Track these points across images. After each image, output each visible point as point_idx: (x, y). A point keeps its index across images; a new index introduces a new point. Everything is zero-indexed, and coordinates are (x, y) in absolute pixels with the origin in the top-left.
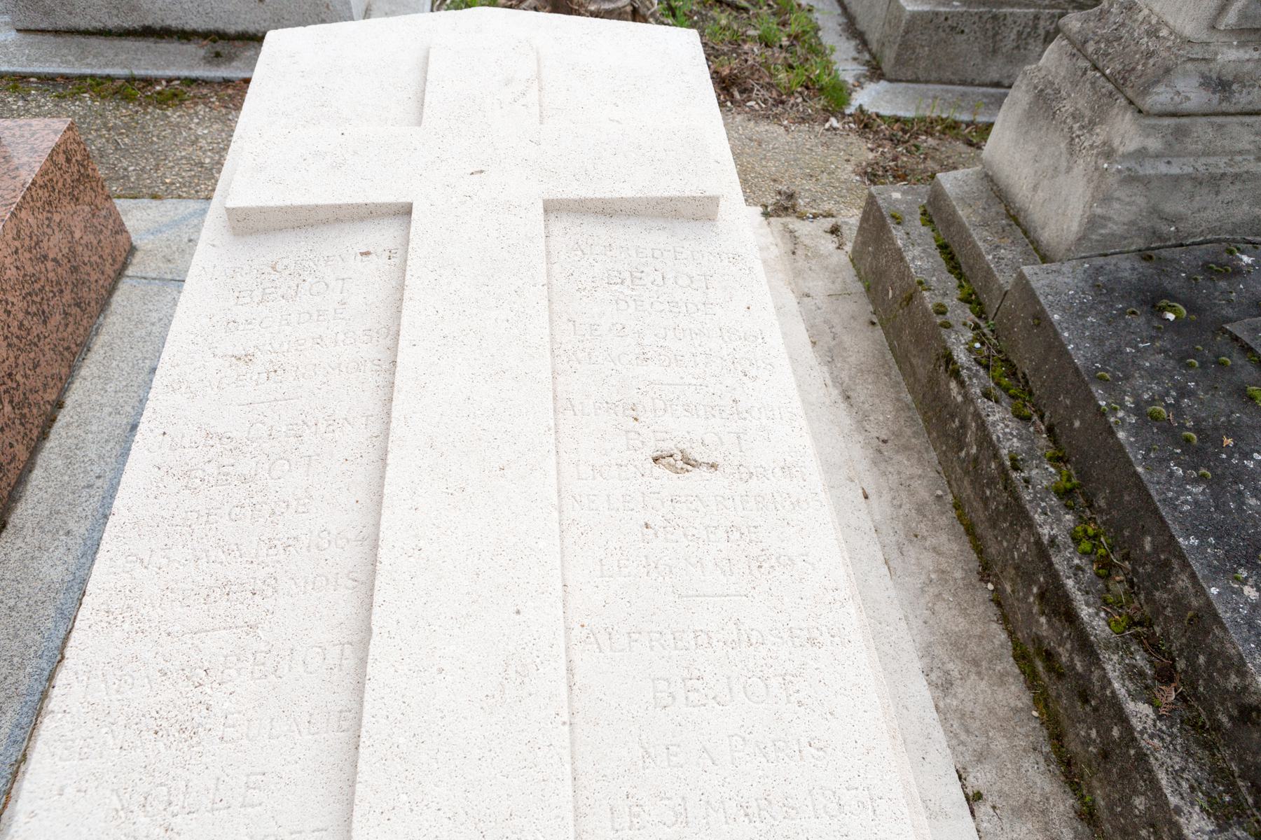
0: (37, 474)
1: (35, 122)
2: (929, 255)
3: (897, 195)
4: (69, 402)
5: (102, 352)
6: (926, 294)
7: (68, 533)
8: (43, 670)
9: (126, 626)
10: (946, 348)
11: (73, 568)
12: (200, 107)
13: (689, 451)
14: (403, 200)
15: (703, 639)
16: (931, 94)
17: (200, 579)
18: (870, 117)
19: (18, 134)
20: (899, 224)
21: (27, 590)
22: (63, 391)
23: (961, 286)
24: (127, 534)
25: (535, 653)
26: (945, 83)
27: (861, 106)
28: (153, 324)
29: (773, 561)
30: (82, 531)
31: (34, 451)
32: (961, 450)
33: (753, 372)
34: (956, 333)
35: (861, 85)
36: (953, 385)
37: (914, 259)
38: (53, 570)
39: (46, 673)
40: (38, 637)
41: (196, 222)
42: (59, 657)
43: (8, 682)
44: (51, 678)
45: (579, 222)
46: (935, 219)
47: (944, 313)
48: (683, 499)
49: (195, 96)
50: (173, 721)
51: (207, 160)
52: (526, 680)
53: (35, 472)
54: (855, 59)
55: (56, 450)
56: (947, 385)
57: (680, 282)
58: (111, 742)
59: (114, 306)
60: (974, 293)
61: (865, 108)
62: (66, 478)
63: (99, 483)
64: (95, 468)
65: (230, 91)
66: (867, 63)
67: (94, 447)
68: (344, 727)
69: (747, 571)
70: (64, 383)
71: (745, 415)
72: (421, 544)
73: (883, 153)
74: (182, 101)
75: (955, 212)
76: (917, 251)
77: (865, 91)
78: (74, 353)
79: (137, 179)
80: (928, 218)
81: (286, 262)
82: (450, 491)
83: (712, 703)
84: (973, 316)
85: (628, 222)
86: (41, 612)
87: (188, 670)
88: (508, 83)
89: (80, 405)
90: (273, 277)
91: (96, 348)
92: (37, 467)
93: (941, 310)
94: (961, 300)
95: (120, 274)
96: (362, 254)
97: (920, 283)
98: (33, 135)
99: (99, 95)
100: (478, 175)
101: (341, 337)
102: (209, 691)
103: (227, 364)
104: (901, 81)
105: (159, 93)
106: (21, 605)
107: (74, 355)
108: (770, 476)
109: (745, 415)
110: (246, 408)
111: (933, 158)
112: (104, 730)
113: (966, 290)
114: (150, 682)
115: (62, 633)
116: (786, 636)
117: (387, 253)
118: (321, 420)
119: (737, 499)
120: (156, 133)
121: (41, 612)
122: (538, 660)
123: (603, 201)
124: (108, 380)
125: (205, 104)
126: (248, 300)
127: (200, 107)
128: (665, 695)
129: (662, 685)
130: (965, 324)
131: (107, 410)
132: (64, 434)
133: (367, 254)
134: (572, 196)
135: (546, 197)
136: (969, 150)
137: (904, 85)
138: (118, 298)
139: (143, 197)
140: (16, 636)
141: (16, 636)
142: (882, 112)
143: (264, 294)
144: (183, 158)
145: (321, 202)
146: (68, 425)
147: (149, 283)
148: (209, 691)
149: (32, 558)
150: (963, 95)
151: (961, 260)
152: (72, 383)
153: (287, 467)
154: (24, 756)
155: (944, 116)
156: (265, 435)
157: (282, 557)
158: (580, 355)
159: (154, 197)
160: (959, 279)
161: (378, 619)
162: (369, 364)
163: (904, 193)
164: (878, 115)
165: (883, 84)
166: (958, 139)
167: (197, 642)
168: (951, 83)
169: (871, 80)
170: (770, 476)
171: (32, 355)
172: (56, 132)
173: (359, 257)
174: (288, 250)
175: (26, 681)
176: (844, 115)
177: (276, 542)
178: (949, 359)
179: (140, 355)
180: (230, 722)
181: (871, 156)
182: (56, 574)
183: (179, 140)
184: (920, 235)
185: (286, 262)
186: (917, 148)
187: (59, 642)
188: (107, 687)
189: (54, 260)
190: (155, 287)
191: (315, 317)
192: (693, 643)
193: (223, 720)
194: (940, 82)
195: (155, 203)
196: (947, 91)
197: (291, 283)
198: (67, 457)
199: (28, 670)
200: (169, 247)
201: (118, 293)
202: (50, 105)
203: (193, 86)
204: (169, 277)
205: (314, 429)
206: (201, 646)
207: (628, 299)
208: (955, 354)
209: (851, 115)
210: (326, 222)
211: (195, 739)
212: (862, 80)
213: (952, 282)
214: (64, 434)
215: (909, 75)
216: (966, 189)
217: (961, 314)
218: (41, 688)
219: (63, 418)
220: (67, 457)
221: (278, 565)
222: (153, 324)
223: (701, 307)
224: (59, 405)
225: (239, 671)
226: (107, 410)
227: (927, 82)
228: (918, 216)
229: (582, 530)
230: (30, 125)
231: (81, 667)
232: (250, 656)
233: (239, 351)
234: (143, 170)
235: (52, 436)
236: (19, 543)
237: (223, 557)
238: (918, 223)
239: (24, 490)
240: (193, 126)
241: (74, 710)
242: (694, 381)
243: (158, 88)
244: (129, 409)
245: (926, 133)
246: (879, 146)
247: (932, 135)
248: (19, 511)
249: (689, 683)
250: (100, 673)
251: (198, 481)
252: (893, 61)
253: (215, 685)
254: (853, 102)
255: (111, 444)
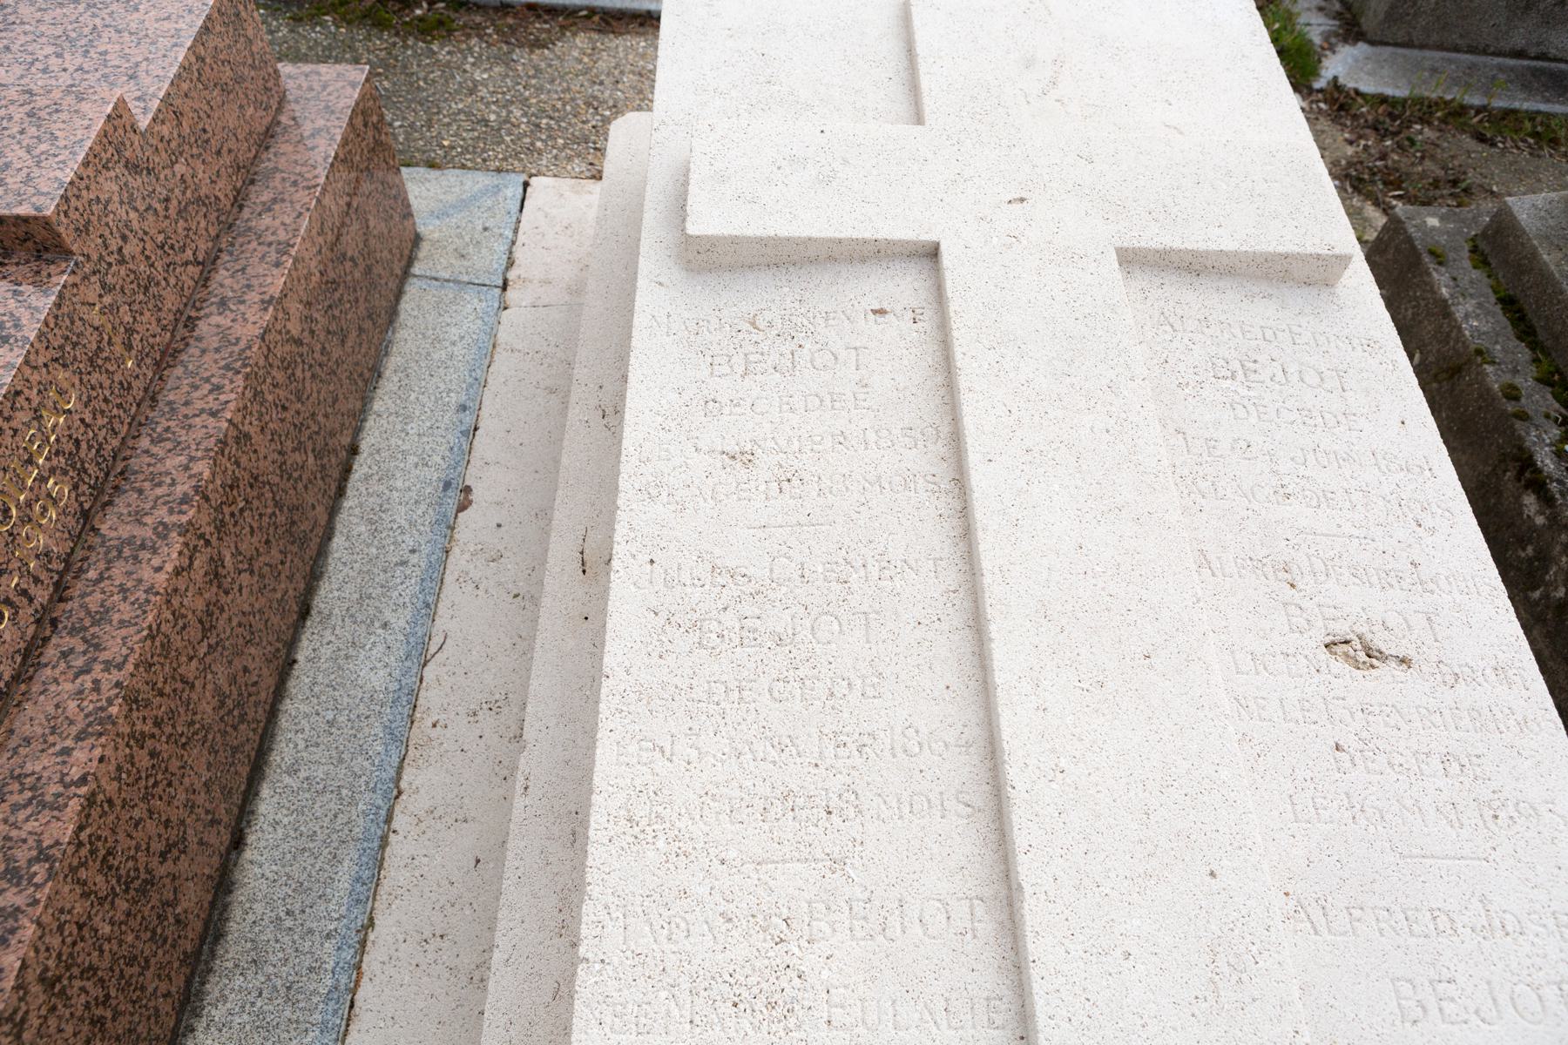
0: (338, 542)
1: (323, 68)
2: (1488, 313)
3: (1433, 222)
4: (364, 446)
5: (396, 379)
6: (1489, 369)
7: (385, 625)
8: (378, 808)
9: (661, 844)
10: (1521, 448)
11: (397, 674)
12: (474, 41)
13: (1369, 636)
14: (925, 237)
15: (1443, 921)
16: (1427, 64)
17: (749, 784)
18: (1348, 94)
19: (305, 85)
20: (1440, 264)
21: (346, 699)
22: (358, 431)
23: (1536, 360)
24: (632, 708)
25: (1249, 938)
26: (1448, 50)
27: (1335, 78)
28: (454, 344)
29: (1511, 810)
30: (402, 623)
31: (333, 511)
32: (1534, 588)
33: (1428, 522)
34: (1537, 427)
35: (1332, 48)
36: (1530, 501)
37: (1467, 316)
38: (375, 671)
39: (383, 812)
40: (366, 763)
41: (489, 203)
42: (395, 792)
43: (339, 821)
44: (389, 819)
45: (1158, 281)
46: (1494, 262)
47: (1517, 399)
48: (1376, 709)
49: (465, 26)
50: (755, 990)
51: (493, 117)
52: (1244, 977)
53: (335, 540)
54: (1321, 9)
55: (357, 511)
56: (1518, 498)
57: (1307, 379)
58: (675, 1012)
59: (402, 316)
60: (1558, 371)
61: (1341, 81)
62: (374, 550)
63: (414, 559)
64: (406, 537)
65: (510, 21)
66: (1338, 16)
67: (403, 509)
68: (998, 1023)
69: (1481, 823)
70: (359, 417)
71: (1431, 586)
72: (1063, 763)
73: (1366, 147)
74: (450, 32)
75: (1535, 254)
76: (1469, 306)
77: (1338, 57)
78: (369, 377)
79: (406, 139)
80: (1480, 257)
81: (768, 315)
82: (1085, 686)
83: (1475, 1020)
84: (1557, 405)
85: (1221, 284)
86: (366, 730)
87: (760, 918)
88: (1029, 63)
89: (378, 451)
90: (755, 338)
91: (387, 373)
92: (337, 533)
93: (1512, 393)
94: (1538, 380)
95: (406, 273)
96: (875, 312)
97: (1479, 352)
98: (324, 87)
99: (343, 19)
100: (1018, 206)
101: (871, 436)
102: (796, 950)
103: (719, 465)
104: (1387, 44)
105: (421, 19)
106: (342, 719)
107: (366, 382)
108: (1481, 679)
109: (1431, 586)
110: (760, 534)
111: (1433, 157)
112: (663, 994)
113: (1545, 367)
114: (710, 929)
115: (395, 761)
116: (1551, 922)
117: (910, 315)
118: (870, 561)
119: (1446, 712)
120: (422, 75)
121: (366, 730)
122: (1254, 948)
123: (1194, 254)
124: (408, 419)
125: (480, 37)
126: (726, 369)
127: (474, 41)
128: (1412, 1003)
129: (1406, 989)
130: (1547, 416)
131: (412, 459)
132: (363, 489)
133: (880, 312)
134: (1153, 245)
135: (1119, 244)
136: (1480, 147)
137: (1390, 49)
138: (406, 305)
139: (417, 165)
140: (341, 761)
141: (341, 761)
142: (1364, 88)
143: (747, 362)
144: (460, 111)
145: (815, 234)
146: (367, 478)
147: (442, 287)
148: (796, 950)
149: (347, 657)
150: (1472, 67)
151: (1539, 324)
152: (364, 420)
153: (836, 627)
154: (371, 919)
155: (1449, 97)
156: (796, 576)
157: (858, 761)
158: (1203, 485)
159: (432, 165)
160: (1533, 349)
161: (1026, 870)
162: (921, 481)
163: (1442, 218)
164: (1357, 92)
165: (1362, 47)
166: (1464, 131)
167: (765, 878)
168: (1457, 49)
169: (1345, 41)
170: (1481, 679)
171: (331, 388)
172: (353, 85)
173: (871, 316)
174: (771, 298)
175: (361, 821)
176: (1311, 91)
177: (845, 738)
178: (1526, 463)
179: (442, 386)
180: (836, 1000)
181: (1350, 150)
182: (378, 680)
183: (453, 87)
184: (1471, 282)
185: (768, 315)
186: (1412, 142)
187: (392, 773)
188: (653, 932)
189: (352, 259)
190: (449, 292)
191: (828, 402)
192: (1432, 927)
193: (824, 995)
194: (1440, 47)
195: (434, 174)
196: (1450, 61)
197: (783, 349)
198: (371, 522)
199: (361, 807)
200: (460, 236)
201: (406, 298)
202: (285, 30)
203: (462, 11)
204: (466, 278)
205: (862, 572)
206: (772, 883)
207: (1246, 402)
208: (1538, 459)
209: (1321, 91)
210: (814, 261)
211: (792, 1021)
212: (1333, 40)
213: (1523, 354)
214: (363, 489)
215: (1401, 36)
216: (1551, 222)
217: (1539, 400)
218: (379, 833)
219: (360, 468)
220: (371, 522)
221: (853, 773)
222: (454, 344)
223: (1341, 418)
224: (354, 450)
225: (832, 925)
226: (412, 459)
227: (1422, 47)
228: (1466, 254)
229: (1258, 749)
230: (318, 73)
231: (611, 899)
232: (843, 904)
233: (732, 448)
234: (412, 125)
235: (349, 492)
236: (328, 636)
237: (773, 753)
238: (1467, 264)
239: (325, 565)
240: (468, 67)
241: (616, 960)
242: (1356, 532)
243: (418, 12)
244: (438, 459)
245: (1422, 121)
246: (1360, 137)
247: (1429, 124)
248: (322, 592)
249: (1441, 987)
250: (639, 910)
251: (714, 636)
252: (1381, 16)
253: (804, 943)
254: (1323, 72)
255: (423, 507)
